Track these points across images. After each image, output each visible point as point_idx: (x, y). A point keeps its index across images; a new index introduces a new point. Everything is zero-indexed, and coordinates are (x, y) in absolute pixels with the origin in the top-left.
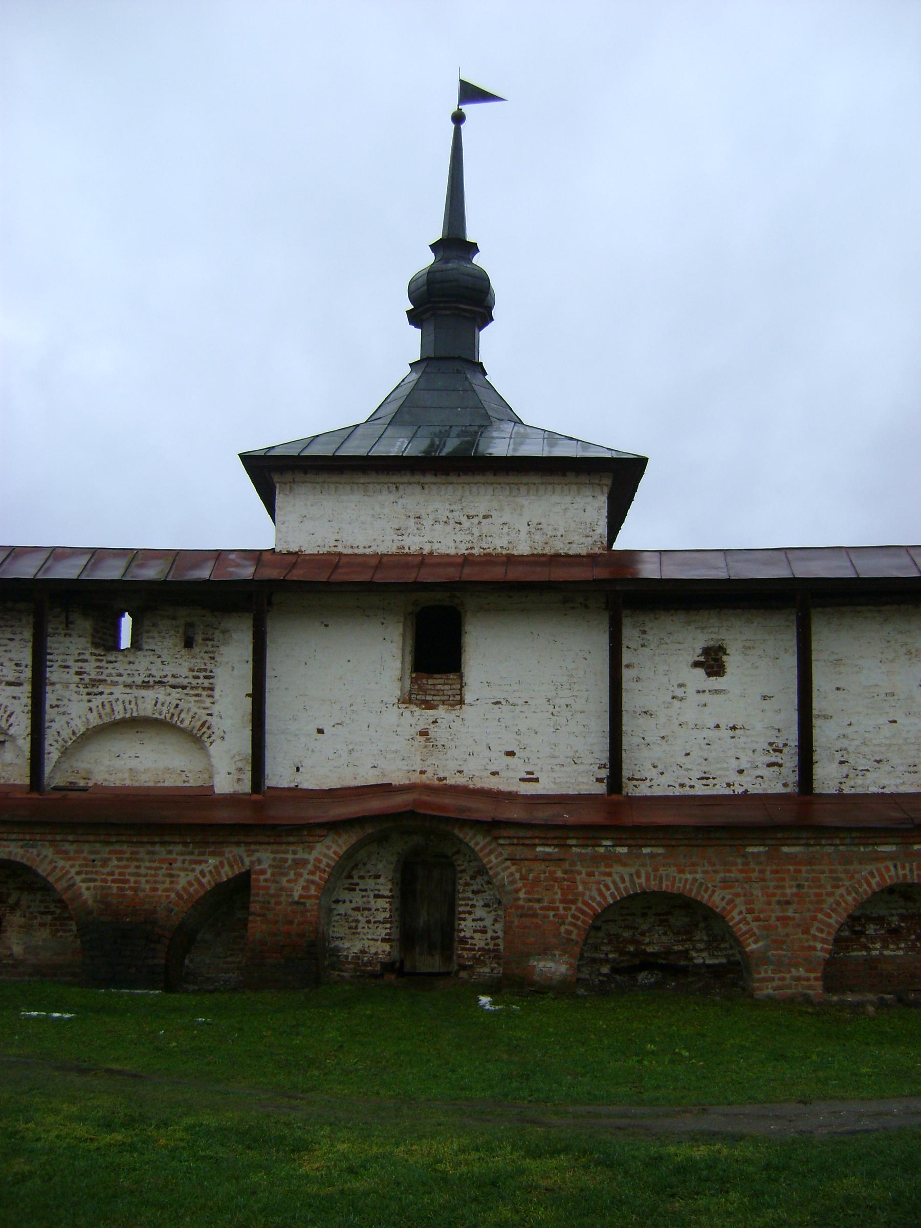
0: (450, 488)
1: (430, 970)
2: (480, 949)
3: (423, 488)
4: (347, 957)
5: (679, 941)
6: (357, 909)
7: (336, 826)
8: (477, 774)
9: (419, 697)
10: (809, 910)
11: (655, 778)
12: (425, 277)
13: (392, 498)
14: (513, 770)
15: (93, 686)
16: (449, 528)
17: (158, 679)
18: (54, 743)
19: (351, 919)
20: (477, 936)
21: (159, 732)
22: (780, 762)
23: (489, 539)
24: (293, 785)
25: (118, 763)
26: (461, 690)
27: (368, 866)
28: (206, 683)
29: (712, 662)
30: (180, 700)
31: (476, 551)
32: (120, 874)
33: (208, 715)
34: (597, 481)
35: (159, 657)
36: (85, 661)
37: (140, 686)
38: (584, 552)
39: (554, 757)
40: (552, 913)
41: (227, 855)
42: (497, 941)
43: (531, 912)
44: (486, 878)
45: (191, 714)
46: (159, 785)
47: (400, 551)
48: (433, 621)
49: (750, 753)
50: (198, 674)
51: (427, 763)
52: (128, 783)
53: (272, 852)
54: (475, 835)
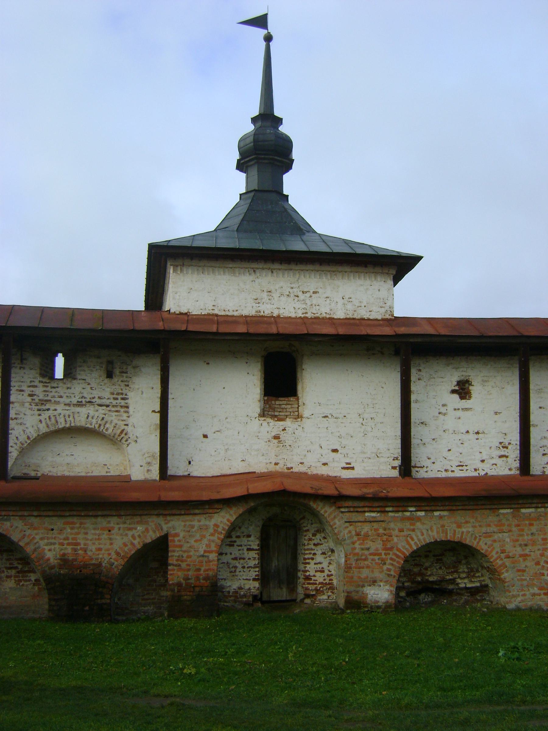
0: (291, 273)
1: (280, 599)
2: (320, 583)
3: (272, 272)
4: (229, 592)
5: (449, 573)
6: (235, 559)
7: (228, 502)
8: (313, 465)
9: (270, 413)
10: (539, 550)
11: (429, 466)
12: (251, 139)
13: (252, 277)
14: (337, 461)
15: (42, 404)
16: (290, 300)
17: (88, 400)
18: (14, 445)
19: (231, 566)
20: (318, 574)
21: (107, 436)
22: (507, 454)
23: (318, 307)
24: (186, 474)
25: (58, 459)
26: (298, 408)
27: (243, 529)
28: (123, 403)
29: (463, 390)
30: (105, 414)
31: (309, 315)
32: (73, 539)
33: (125, 425)
34: (387, 271)
35: (89, 384)
36: (36, 386)
37: (76, 405)
38: (379, 317)
39: (364, 453)
40: (376, 557)
41: (150, 524)
42: (331, 577)
43: (363, 557)
44: (323, 535)
45: (113, 424)
46: (89, 475)
47: (258, 314)
48: (281, 361)
49: (488, 448)
50: (117, 396)
51: (279, 458)
52: (67, 474)
53: (183, 521)
54: (324, 506)
